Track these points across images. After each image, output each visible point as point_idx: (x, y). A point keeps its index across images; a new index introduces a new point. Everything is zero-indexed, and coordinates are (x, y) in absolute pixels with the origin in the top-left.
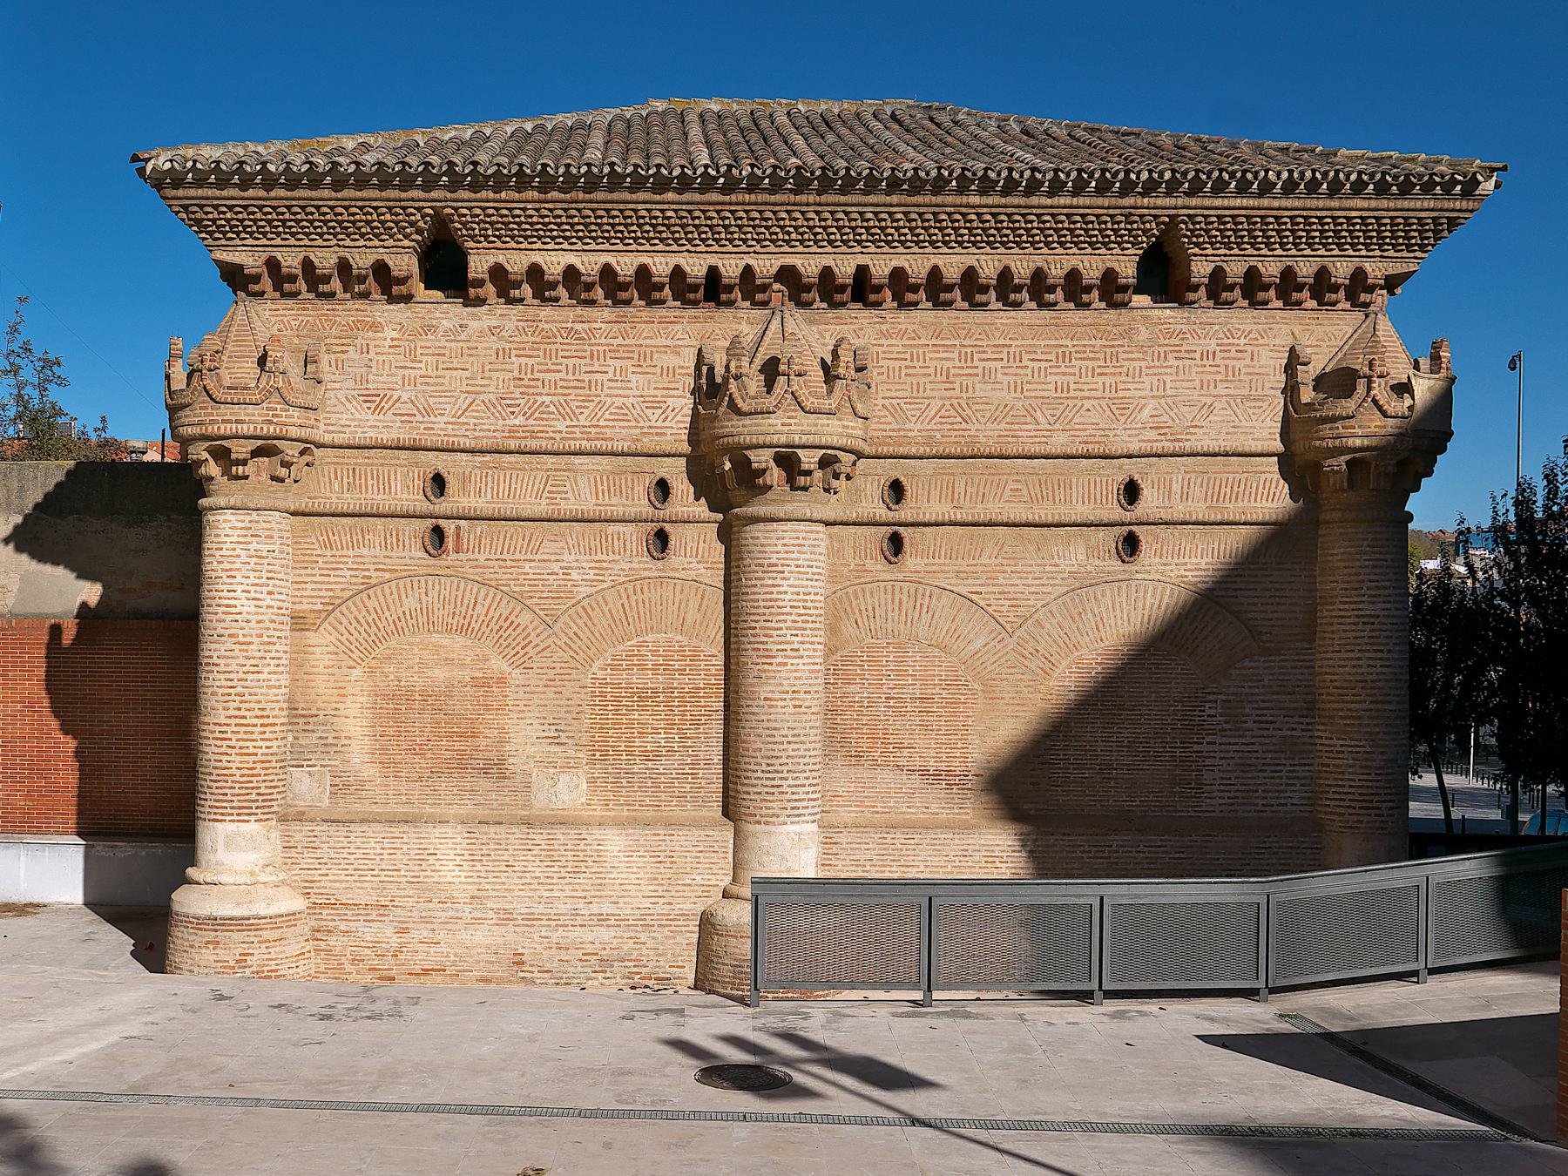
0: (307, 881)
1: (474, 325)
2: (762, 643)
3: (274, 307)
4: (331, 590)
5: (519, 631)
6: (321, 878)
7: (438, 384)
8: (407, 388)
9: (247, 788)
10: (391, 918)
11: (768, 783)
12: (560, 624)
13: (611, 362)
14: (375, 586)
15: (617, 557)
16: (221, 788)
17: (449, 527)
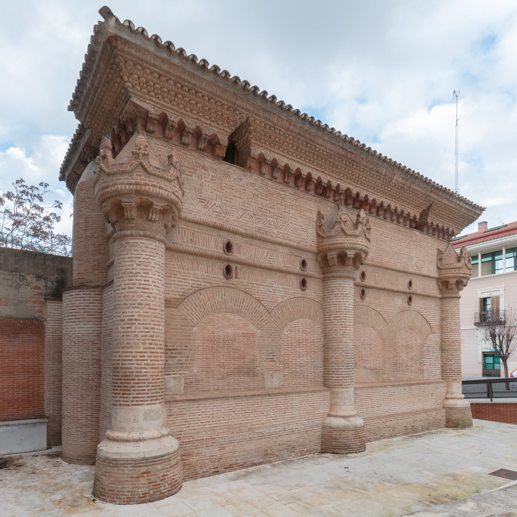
0: (179, 431)
1: (245, 180)
2: (343, 322)
3: (156, 142)
4: (183, 289)
5: (259, 314)
6: (186, 429)
7: (231, 202)
8: (218, 200)
9: (155, 386)
10: (217, 443)
11: (347, 373)
12: (273, 313)
13: (291, 210)
14: (203, 289)
15: (290, 288)
16: (141, 387)
17: (233, 266)
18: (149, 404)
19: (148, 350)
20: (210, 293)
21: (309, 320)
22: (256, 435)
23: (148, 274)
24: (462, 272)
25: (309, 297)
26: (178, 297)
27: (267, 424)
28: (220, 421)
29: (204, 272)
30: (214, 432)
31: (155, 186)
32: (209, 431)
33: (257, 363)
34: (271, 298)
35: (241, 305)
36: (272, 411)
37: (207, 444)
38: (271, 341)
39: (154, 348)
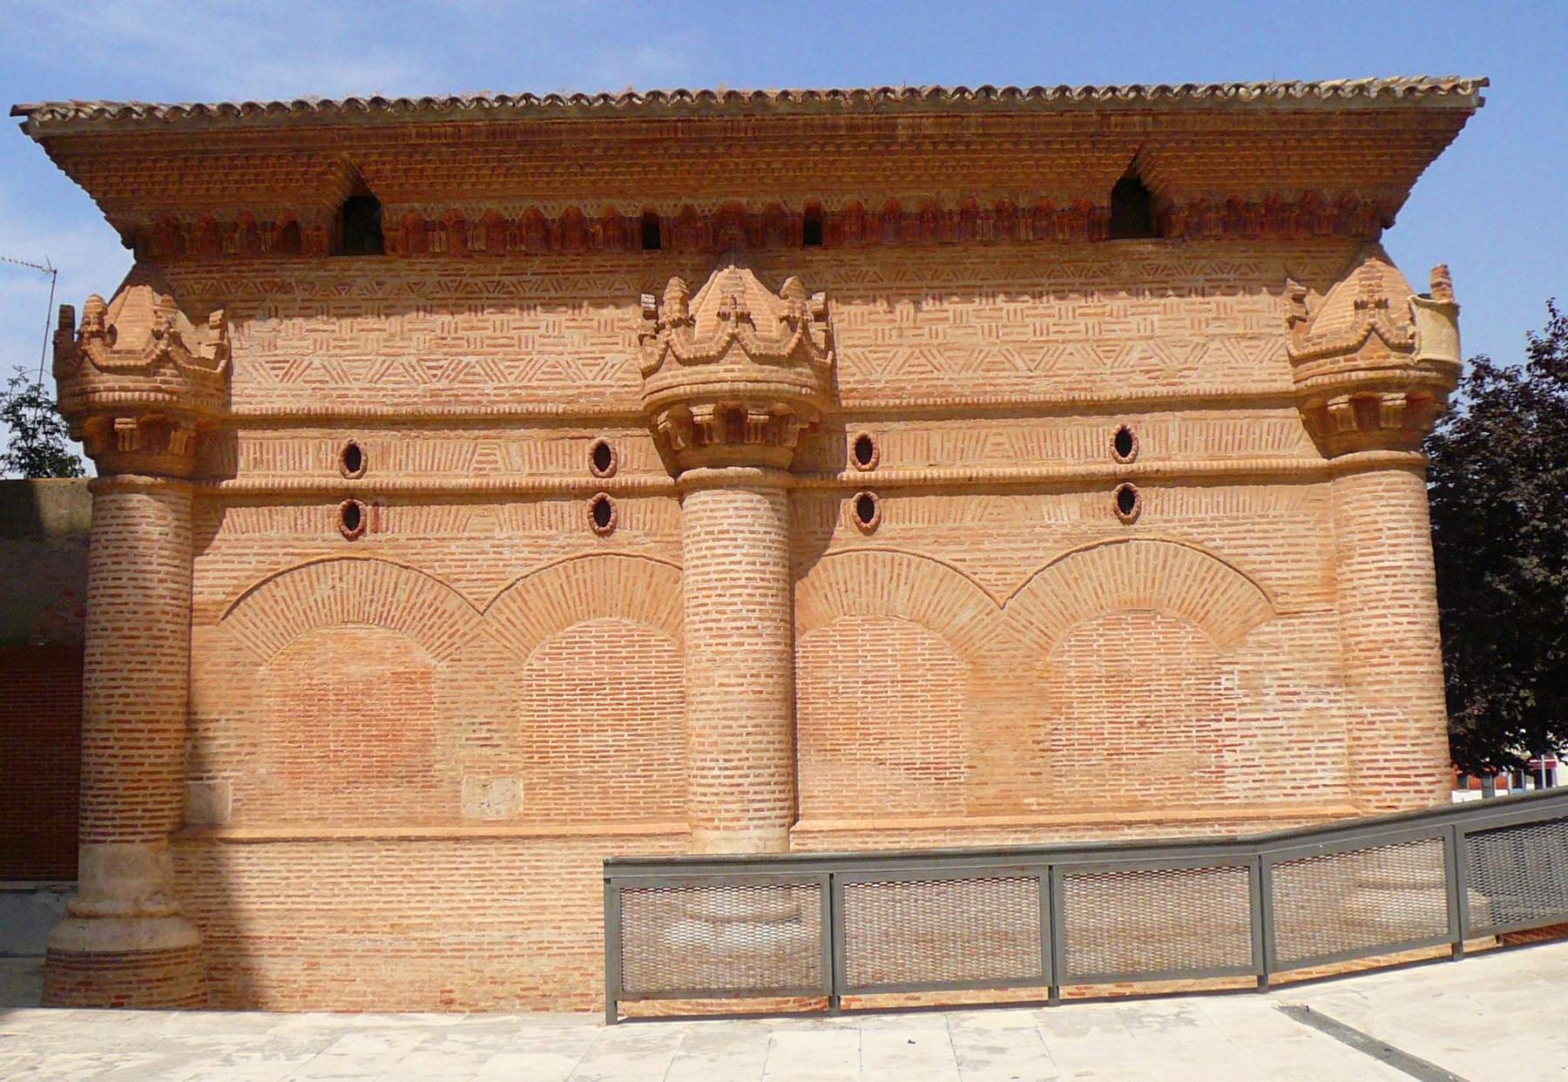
0: (202, 911)
4: (234, 578)
10: (300, 951)
18: (113, 842)
19: (115, 726)
20: (302, 580)
22: (414, 945)
23: (120, 563)
24: (1362, 364)
25: (625, 551)
26: (221, 597)
27: (446, 920)
28: (308, 896)
29: (287, 530)
30: (292, 923)
31: (112, 390)
33: (435, 752)
34: (485, 569)
37: (273, 949)
38: (482, 690)
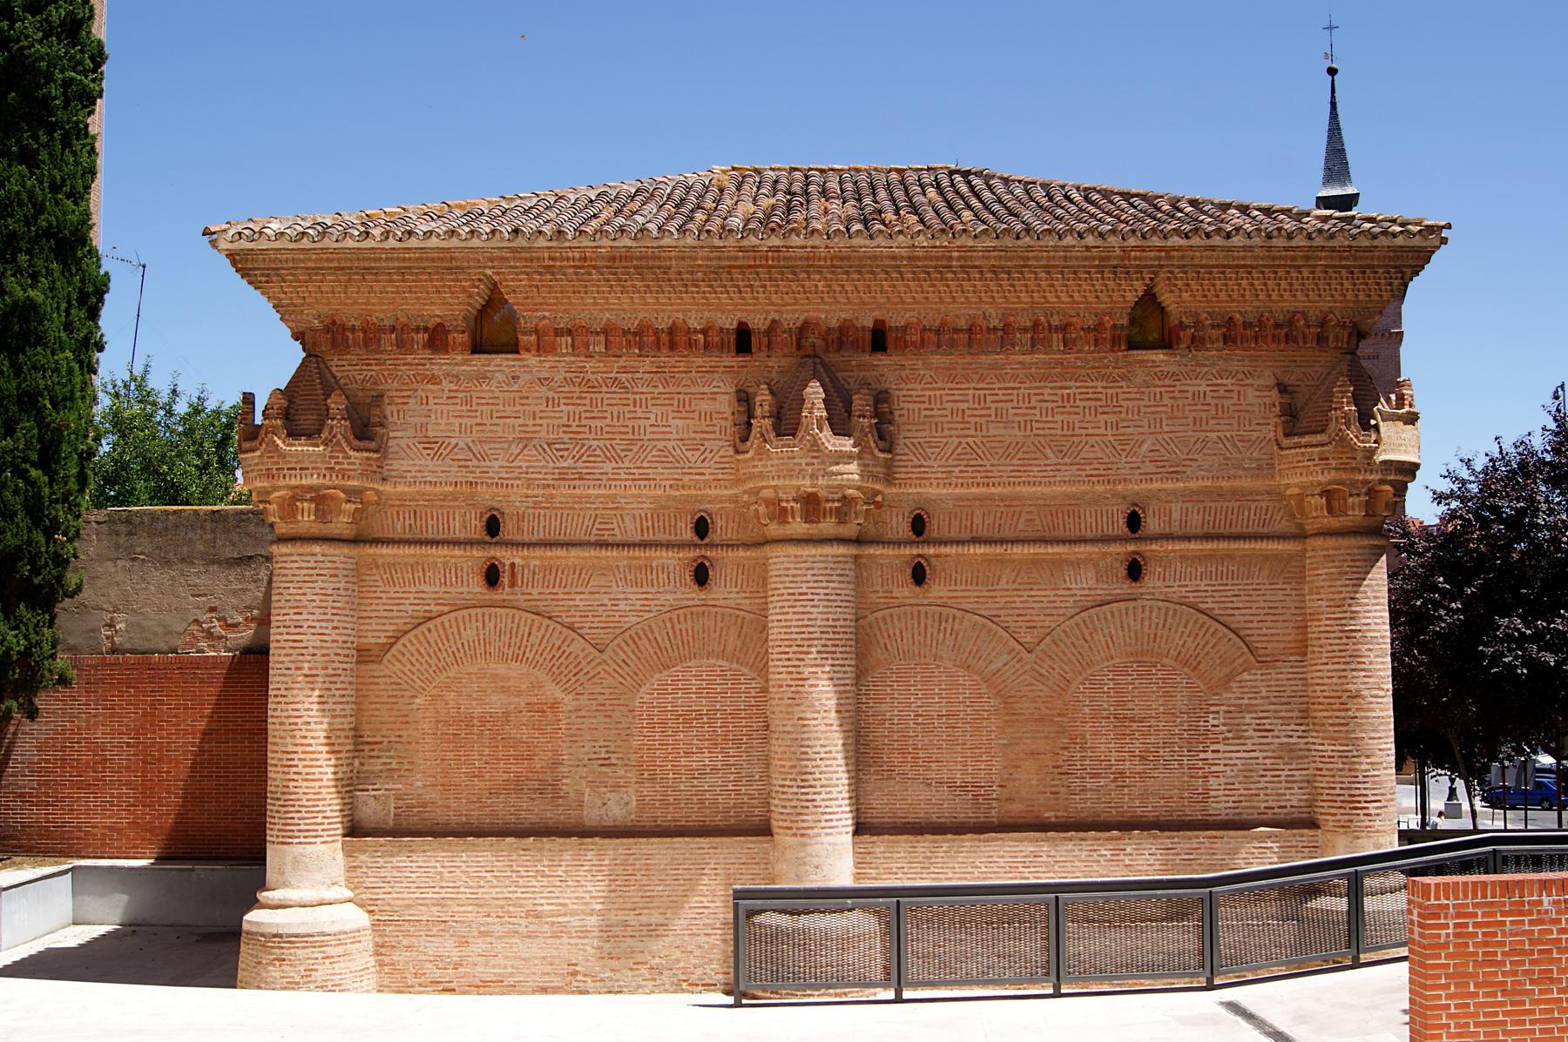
21: (720, 663)
32: (434, 905)
34: (604, 619)
35: (524, 643)
36: (590, 878)
39: (310, 745)
